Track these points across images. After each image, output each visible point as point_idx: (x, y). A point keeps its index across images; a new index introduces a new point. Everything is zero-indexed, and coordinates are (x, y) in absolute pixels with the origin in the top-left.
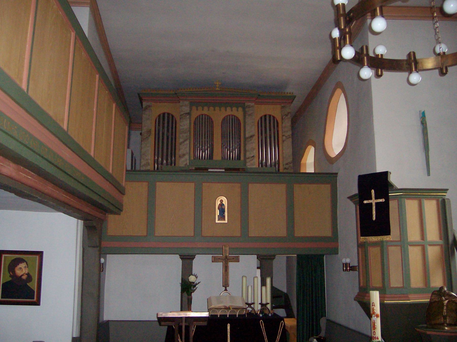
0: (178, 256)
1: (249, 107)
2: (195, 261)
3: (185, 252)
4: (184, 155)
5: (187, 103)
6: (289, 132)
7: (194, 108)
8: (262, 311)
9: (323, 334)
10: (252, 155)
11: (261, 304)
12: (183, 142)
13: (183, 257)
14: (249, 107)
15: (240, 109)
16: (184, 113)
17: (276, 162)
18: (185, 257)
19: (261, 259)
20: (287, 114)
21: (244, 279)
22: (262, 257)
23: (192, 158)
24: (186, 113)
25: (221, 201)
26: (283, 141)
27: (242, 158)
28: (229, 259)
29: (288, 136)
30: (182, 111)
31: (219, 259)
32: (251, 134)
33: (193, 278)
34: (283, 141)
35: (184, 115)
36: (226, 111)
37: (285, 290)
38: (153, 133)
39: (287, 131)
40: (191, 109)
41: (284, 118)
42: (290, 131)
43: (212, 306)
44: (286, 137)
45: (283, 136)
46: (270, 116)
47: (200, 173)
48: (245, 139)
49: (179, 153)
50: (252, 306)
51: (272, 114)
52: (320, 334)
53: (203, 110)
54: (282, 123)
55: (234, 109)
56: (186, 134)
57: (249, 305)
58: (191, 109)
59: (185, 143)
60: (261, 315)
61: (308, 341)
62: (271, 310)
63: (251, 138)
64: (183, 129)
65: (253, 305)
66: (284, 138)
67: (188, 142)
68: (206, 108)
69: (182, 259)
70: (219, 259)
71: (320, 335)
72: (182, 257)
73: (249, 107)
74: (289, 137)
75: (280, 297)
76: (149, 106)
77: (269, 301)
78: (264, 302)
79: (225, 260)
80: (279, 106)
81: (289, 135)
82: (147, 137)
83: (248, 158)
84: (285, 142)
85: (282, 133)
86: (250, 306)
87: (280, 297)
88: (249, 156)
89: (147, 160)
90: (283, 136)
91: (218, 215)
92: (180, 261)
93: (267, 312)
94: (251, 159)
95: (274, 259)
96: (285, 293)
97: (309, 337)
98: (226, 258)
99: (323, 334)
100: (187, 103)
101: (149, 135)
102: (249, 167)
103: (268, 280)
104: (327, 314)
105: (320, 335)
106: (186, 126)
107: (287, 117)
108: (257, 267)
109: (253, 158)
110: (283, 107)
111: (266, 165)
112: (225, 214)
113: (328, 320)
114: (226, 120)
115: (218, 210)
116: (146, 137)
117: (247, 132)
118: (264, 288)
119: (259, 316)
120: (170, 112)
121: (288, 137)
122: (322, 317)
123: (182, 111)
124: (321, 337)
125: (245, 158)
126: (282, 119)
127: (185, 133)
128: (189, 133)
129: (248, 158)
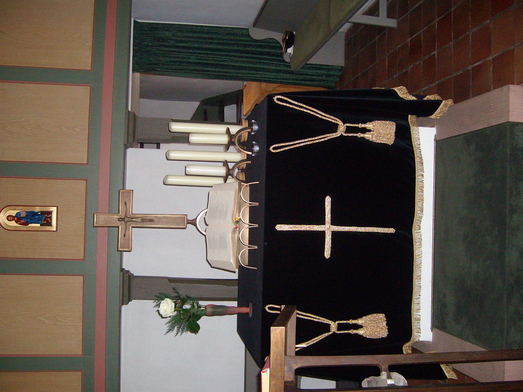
0: (124, 307)
2: (136, 272)
3: (116, 293)
8: (246, 145)
9: (279, 37)
11: (227, 147)
13: (126, 298)
18: (126, 292)
19: (134, 140)
21: (171, 180)
22: (131, 139)
25: (9, 218)
28: (126, 212)
31: (125, 235)
33: (166, 307)
37: (196, 104)
43: (232, 261)
50: (231, 166)
52: (278, 42)
57: (229, 173)
60: (257, 148)
61: (289, 63)
62: (242, 125)
65: (228, 163)
69: (129, 300)
70: (125, 235)
71: (280, 40)
72: (126, 299)
75: (205, 112)
77: (222, 128)
78: (225, 139)
79: (128, 223)
86: (231, 172)
87: (205, 112)
91: (39, 225)
92: (134, 303)
93: (245, 136)
95: (134, 115)
96: (200, 105)
97: (284, 61)
98: (123, 219)
99: (279, 37)
103: (176, 127)
104: (243, 26)
105: (280, 40)
108: (157, 149)
112: (39, 212)
113: (255, 24)
115: (30, 225)
118: (193, 138)
119: (258, 152)
122: (249, 35)
124: (284, 40)
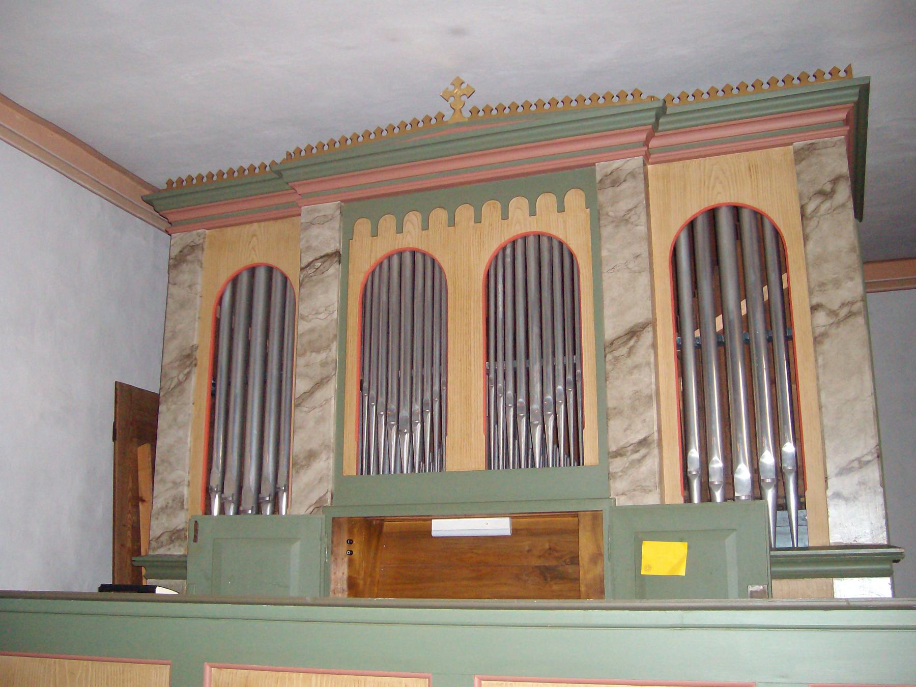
1: (615, 181)
4: (312, 456)
5: (330, 208)
6: (850, 284)
7: (363, 227)
10: (640, 437)
12: (311, 393)
14: (615, 181)
15: (575, 199)
16: (318, 255)
17: (580, 369)
20: (828, 188)
23: (350, 468)
24: (327, 256)
26: (817, 340)
27: (590, 455)
29: (843, 305)
30: (309, 248)
32: (638, 315)
34: (817, 340)
35: (318, 264)
36: (505, 216)
38: (204, 358)
39: (837, 283)
40: (348, 235)
41: (810, 208)
42: (852, 279)
44: (833, 313)
45: (814, 308)
46: (736, 210)
47: (615, 131)
48: (605, 348)
49: (299, 444)
51: (745, 197)
53: (400, 230)
54: (806, 238)
55: (546, 201)
56: (322, 356)
58: (348, 235)
59: (319, 395)
63: (632, 343)
64: (312, 330)
66: (822, 318)
67: (330, 390)
68: (413, 220)
73: (615, 183)
74: (851, 314)
76: (193, 248)
80: (781, 155)
81: (852, 303)
82: (180, 383)
83: (619, 454)
84: (826, 346)
85: (811, 292)
88: (621, 444)
89: (176, 484)
90: (814, 308)
94: (636, 456)
100: (330, 208)
101: (186, 371)
102: (622, 501)
106: (322, 316)
107: (827, 205)
109: (643, 451)
110: (800, 156)
111: (730, 496)
114: (509, 260)
116: (175, 381)
117: (608, 311)
120: (271, 262)
121: (843, 312)
123: (309, 248)
125: (609, 455)
126: (803, 215)
127: (318, 351)
128: (334, 346)
129: (619, 454)
